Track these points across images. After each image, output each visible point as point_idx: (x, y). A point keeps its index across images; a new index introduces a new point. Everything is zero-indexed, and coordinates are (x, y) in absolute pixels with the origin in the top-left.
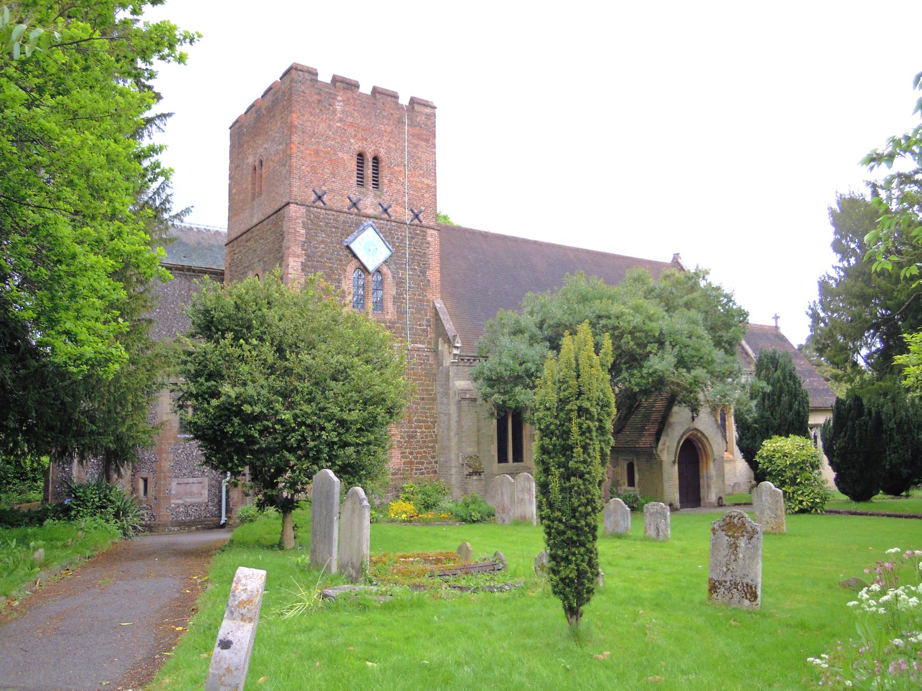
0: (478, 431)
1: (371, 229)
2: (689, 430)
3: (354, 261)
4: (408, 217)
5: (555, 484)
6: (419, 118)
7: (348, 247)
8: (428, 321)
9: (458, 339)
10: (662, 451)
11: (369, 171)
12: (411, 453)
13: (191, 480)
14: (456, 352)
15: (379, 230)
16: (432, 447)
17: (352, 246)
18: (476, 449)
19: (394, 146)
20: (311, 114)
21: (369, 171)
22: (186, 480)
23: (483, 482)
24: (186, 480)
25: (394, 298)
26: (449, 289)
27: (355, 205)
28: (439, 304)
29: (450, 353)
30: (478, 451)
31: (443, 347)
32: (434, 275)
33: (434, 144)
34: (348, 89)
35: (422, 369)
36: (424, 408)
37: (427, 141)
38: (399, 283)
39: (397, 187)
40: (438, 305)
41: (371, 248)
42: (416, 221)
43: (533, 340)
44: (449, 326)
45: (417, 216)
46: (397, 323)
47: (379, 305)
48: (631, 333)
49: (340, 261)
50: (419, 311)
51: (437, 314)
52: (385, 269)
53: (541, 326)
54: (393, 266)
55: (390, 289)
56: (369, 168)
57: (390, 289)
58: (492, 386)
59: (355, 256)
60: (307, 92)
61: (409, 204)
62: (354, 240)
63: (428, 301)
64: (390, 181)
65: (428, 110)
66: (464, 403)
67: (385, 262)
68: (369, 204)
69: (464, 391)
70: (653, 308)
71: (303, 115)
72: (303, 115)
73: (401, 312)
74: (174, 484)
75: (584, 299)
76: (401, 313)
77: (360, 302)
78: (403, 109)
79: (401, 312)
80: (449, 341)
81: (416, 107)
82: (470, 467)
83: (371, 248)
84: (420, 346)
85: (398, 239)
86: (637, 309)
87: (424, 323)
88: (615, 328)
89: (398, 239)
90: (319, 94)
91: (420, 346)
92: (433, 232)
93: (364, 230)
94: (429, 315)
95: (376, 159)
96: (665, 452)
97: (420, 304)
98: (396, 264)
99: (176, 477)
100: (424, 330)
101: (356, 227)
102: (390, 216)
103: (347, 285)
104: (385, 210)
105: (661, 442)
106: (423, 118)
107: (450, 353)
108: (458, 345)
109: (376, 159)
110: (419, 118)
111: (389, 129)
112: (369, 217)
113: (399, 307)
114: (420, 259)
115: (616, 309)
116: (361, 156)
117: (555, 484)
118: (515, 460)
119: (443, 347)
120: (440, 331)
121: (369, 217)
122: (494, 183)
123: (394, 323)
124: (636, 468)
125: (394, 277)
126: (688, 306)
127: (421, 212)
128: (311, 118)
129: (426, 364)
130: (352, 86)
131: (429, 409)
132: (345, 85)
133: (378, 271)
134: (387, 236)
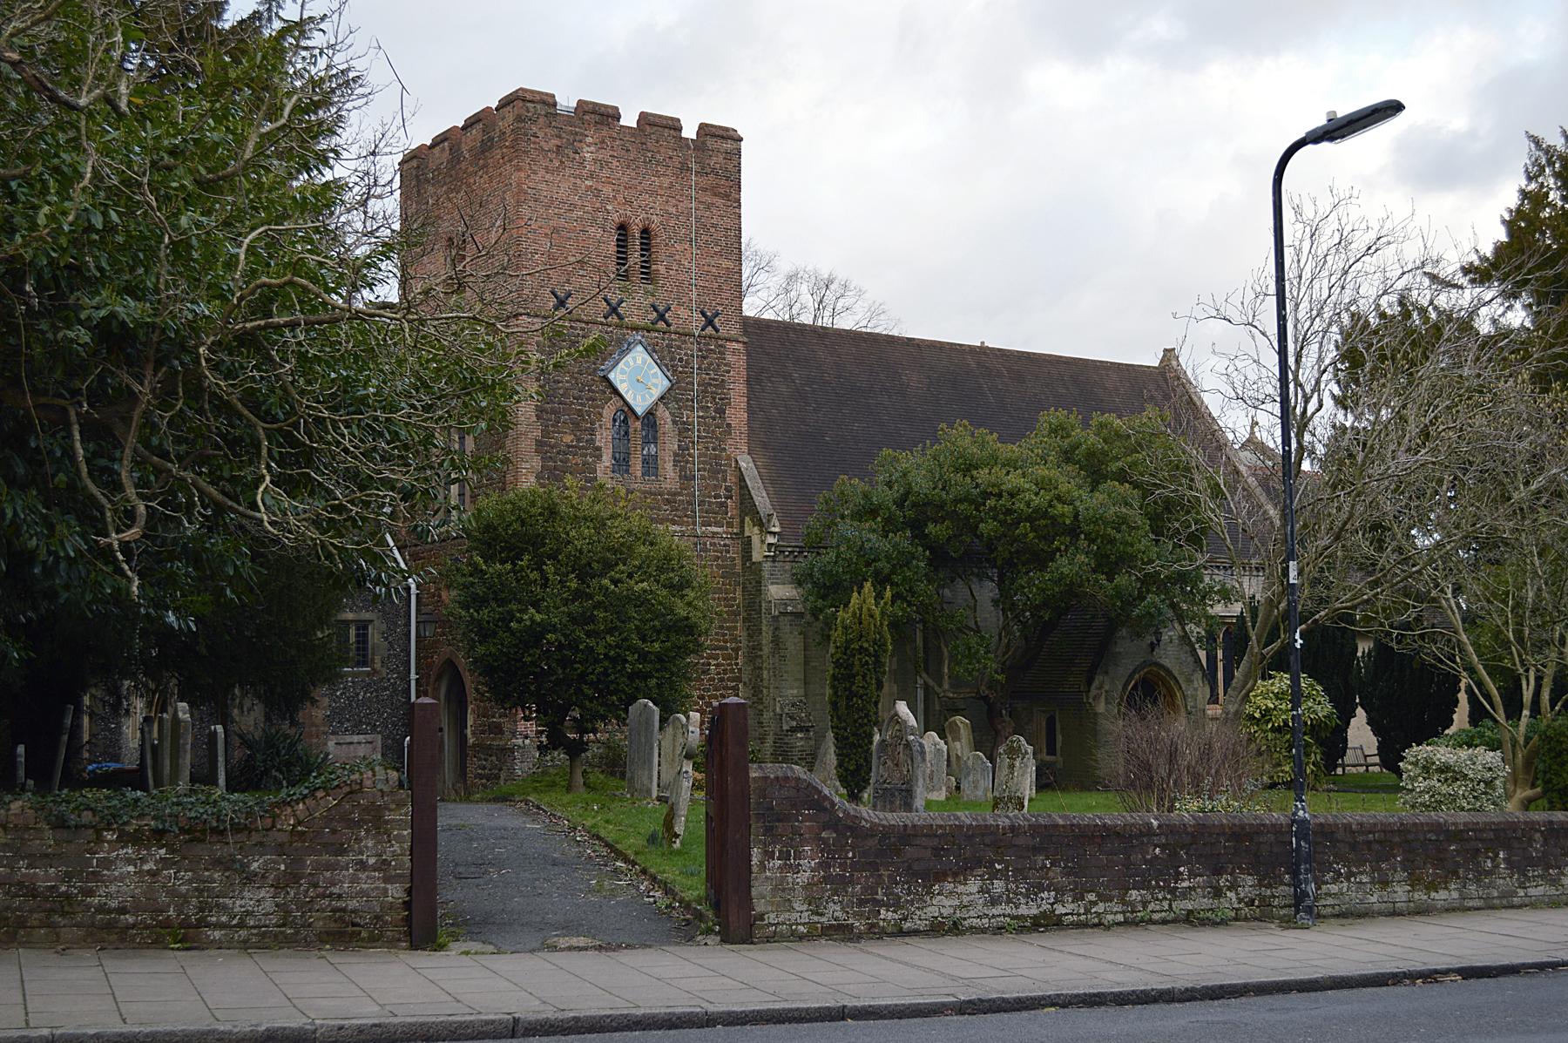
0: (806, 663)
1: (640, 348)
2: (1144, 664)
3: (615, 398)
4: (696, 323)
5: (842, 704)
6: (718, 150)
7: (606, 379)
8: (728, 489)
9: (775, 520)
10: (1096, 698)
11: (635, 257)
12: (701, 697)
13: (356, 738)
14: (771, 540)
15: (652, 350)
16: (732, 688)
17: (611, 376)
18: (802, 692)
19: (674, 210)
20: (547, 169)
21: (635, 257)
22: (348, 739)
23: (812, 742)
24: (348, 739)
25: (676, 455)
26: (760, 442)
27: (614, 310)
28: (745, 463)
29: (763, 542)
30: (806, 695)
31: (752, 531)
32: (737, 415)
33: (738, 201)
34: (602, 124)
35: (718, 566)
36: (721, 627)
37: (727, 196)
38: (683, 429)
39: (679, 261)
40: (743, 465)
41: (638, 378)
42: (709, 330)
43: (890, 526)
44: (762, 500)
45: (710, 322)
46: (680, 494)
47: (651, 465)
48: (1029, 519)
49: (594, 400)
50: (714, 473)
51: (742, 479)
52: (664, 415)
53: (900, 503)
54: (673, 405)
55: (670, 443)
56: (635, 247)
57: (670, 443)
58: (824, 597)
59: (616, 392)
60: (541, 134)
61: (698, 303)
62: (614, 366)
63: (728, 458)
64: (668, 269)
65: (728, 145)
66: (784, 621)
67: (662, 398)
68: (636, 307)
69: (784, 602)
70: (1068, 481)
71: (535, 173)
72: (535, 173)
73: (686, 478)
74: (331, 744)
75: (968, 467)
76: (686, 478)
77: (622, 463)
78: (688, 146)
79: (686, 478)
80: (760, 524)
81: (710, 142)
82: (792, 718)
83: (638, 378)
84: (715, 529)
85: (681, 360)
86: (1042, 485)
87: (722, 492)
88: (1009, 512)
89: (681, 360)
90: (559, 137)
91: (715, 529)
92: (735, 345)
93: (629, 350)
94: (731, 479)
95: (645, 232)
96: (1103, 699)
97: (715, 466)
98: (677, 401)
99: (333, 733)
100: (722, 504)
101: (615, 348)
102: (668, 325)
103: (604, 438)
104: (661, 317)
105: (1096, 683)
106: (721, 160)
107: (763, 542)
108: (777, 530)
109: (645, 232)
110: (718, 150)
111: (666, 182)
112: (636, 329)
113: (683, 469)
114: (715, 393)
115: (1013, 480)
116: (623, 228)
117: (842, 704)
118: (156, 786)
119: (752, 531)
120: (747, 506)
121: (636, 329)
122: (858, 222)
123: (675, 494)
124: (1058, 726)
125: (674, 422)
126: (1122, 476)
127: (717, 315)
128: (548, 176)
129: (724, 559)
130: (608, 116)
131: (728, 628)
132: (597, 118)
133: (650, 413)
134: (664, 357)
